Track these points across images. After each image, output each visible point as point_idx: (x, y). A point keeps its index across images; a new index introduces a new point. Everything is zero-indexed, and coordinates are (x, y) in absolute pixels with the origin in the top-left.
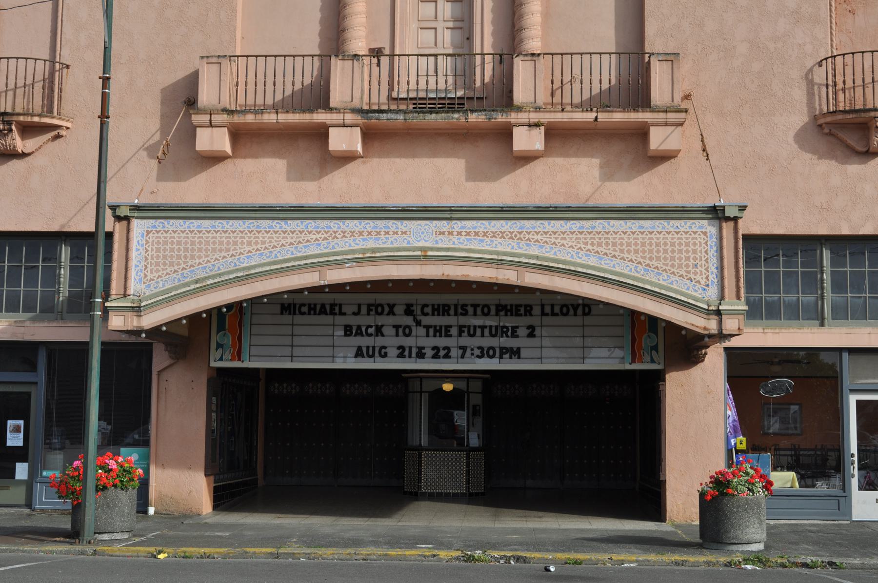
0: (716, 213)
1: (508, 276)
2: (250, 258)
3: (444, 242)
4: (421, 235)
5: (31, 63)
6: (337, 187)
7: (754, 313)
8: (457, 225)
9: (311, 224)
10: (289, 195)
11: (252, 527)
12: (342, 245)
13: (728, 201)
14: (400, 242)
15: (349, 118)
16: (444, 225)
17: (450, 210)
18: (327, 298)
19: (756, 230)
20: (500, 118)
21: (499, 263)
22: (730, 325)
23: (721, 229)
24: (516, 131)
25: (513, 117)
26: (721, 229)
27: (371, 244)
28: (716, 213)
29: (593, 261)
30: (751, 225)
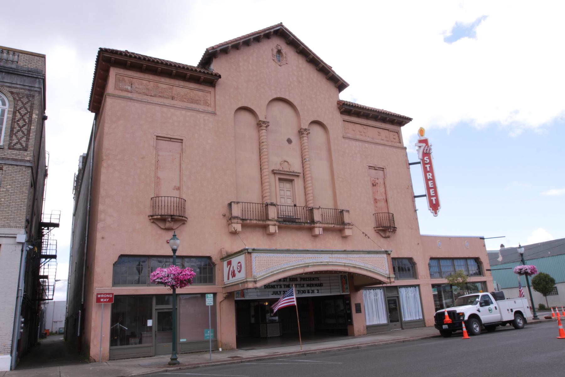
0: (386, 252)
1: (347, 269)
2: (285, 266)
3: (334, 260)
4: (325, 258)
5: (166, 198)
6: (319, 245)
7: (396, 278)
8: (334, 255)
9: (299, 255)
10: (309, 247)
11: (284, 356)
12: (307, 261)
13: (389, 249)
14: (319, 260)
15: (275, 223)
16: (330, 256)
17: (332, 251)
18: (312, 276)
19: (396, 256)
20: (313, 225)
21: (345, 266)
22: (392, 280)
23: (60, 334)
24: (271, 227)
25: (268, 222)
26: (60, 334)
27: (315, 261)
28: (386, 252)
29: (363, 265)
30: (393, 255)
